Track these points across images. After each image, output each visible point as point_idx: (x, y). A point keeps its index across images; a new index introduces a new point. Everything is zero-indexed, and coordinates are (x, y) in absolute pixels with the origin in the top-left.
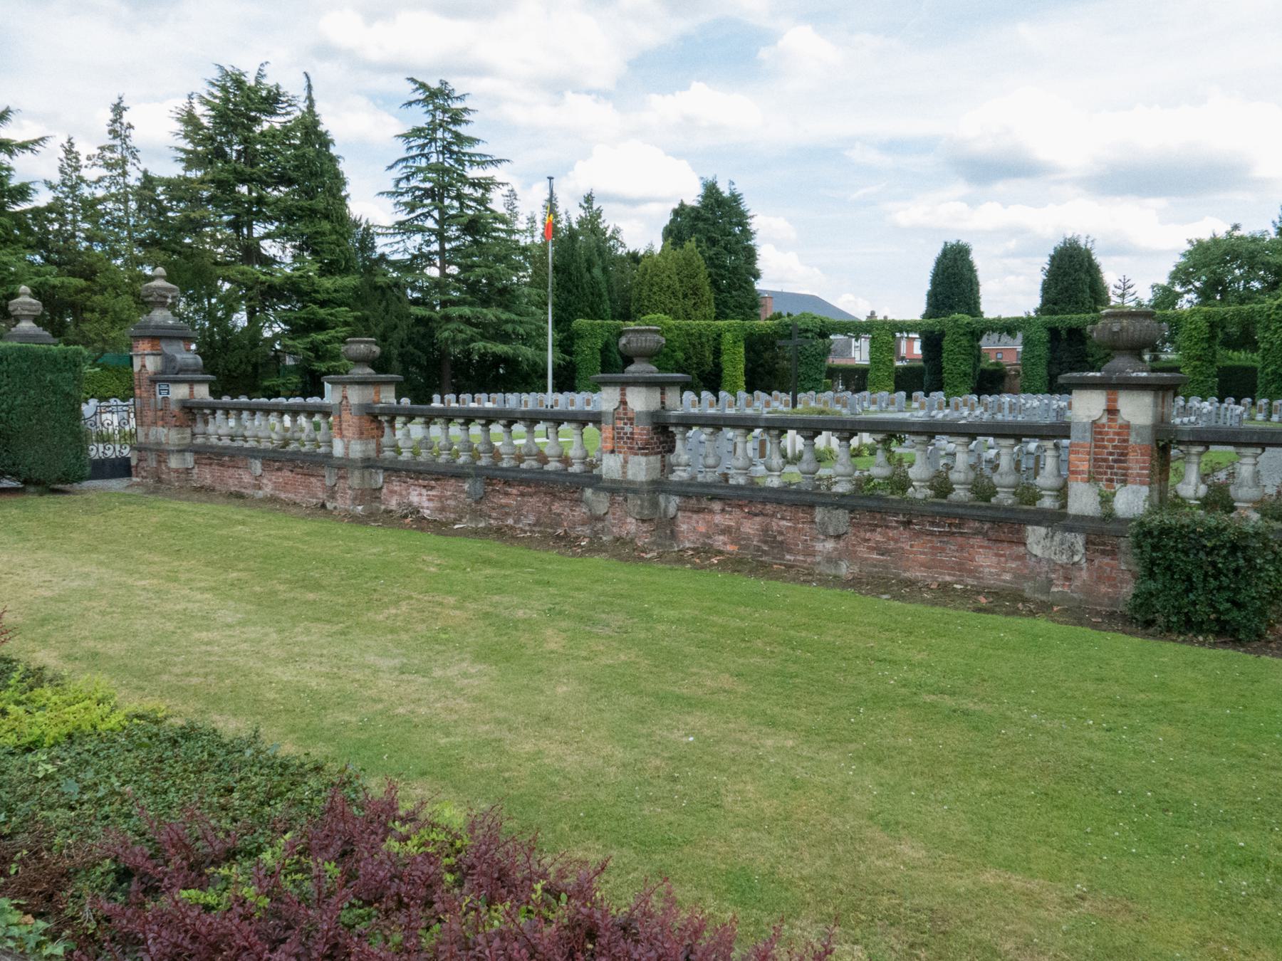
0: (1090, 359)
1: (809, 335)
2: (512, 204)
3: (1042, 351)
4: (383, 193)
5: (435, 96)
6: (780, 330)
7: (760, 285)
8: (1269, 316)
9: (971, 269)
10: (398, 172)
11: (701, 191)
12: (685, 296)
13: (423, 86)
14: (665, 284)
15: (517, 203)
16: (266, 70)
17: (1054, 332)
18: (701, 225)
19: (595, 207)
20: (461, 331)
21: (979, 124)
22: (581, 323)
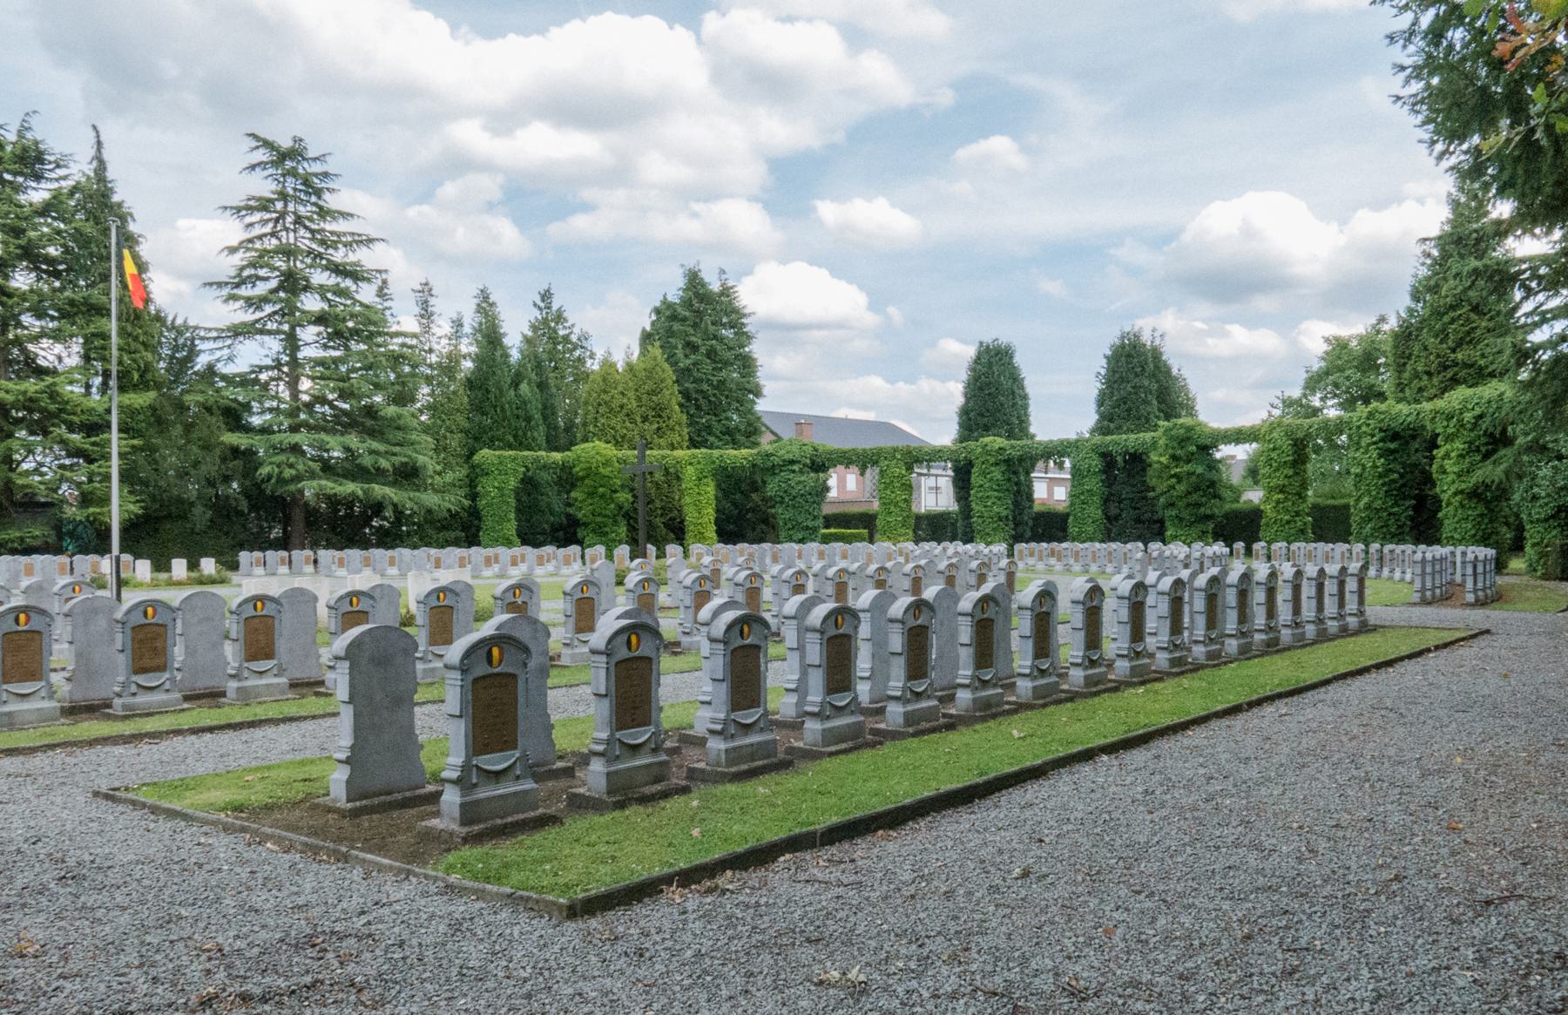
0: (1151, 494)
1: (796, 467)
2: (426, 302)
3: (1094, 484)
4: (211, 284)
5: (285, 157)
6: (759, 462)
7: (761, 406)
8: (1359, 427)
9: (1016, 378)
10: (238, 259)
11: (681, 282)
12: (645, 419)
13: (267, 144)
14: (615, 404)
15: (432, 301)
16: (34, 121)
17: (1107, 458)
18: (677, 326)
19: (555, 308)
20: (291, 466)
21: (1221, 223)
22: (485, 455)
